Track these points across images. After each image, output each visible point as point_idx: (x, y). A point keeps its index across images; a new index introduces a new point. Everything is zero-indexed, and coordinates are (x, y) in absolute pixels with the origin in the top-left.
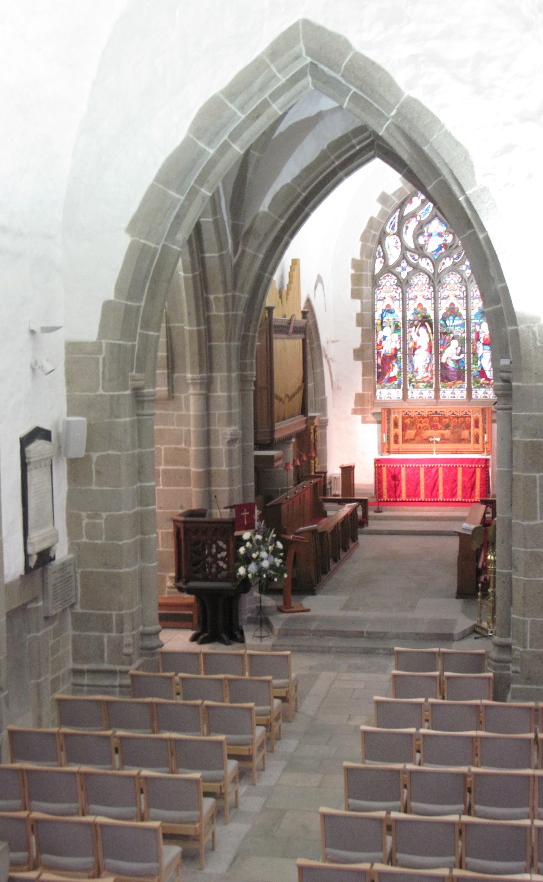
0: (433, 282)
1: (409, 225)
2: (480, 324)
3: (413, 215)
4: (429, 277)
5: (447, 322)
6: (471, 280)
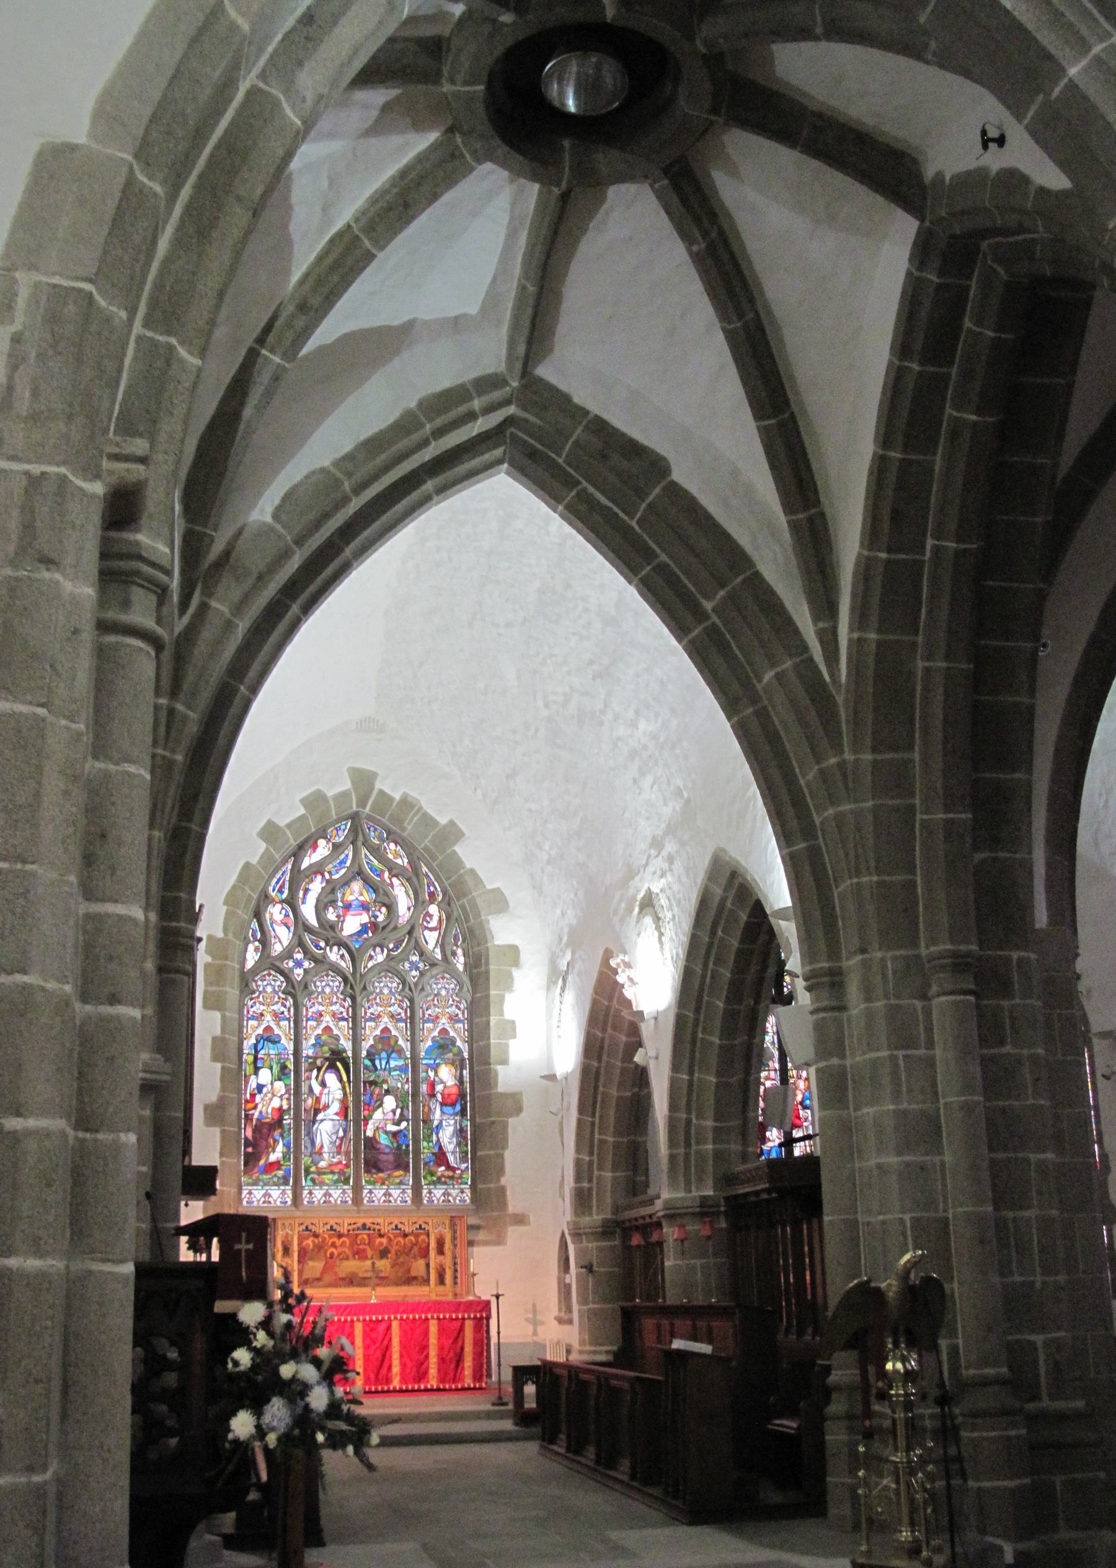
0: (352, 987)
1: (311, 886)
2: (435, 1068)
3: (318, 869)
4: (345, 979)
5: (377, 1062)
6: (420, 987)
